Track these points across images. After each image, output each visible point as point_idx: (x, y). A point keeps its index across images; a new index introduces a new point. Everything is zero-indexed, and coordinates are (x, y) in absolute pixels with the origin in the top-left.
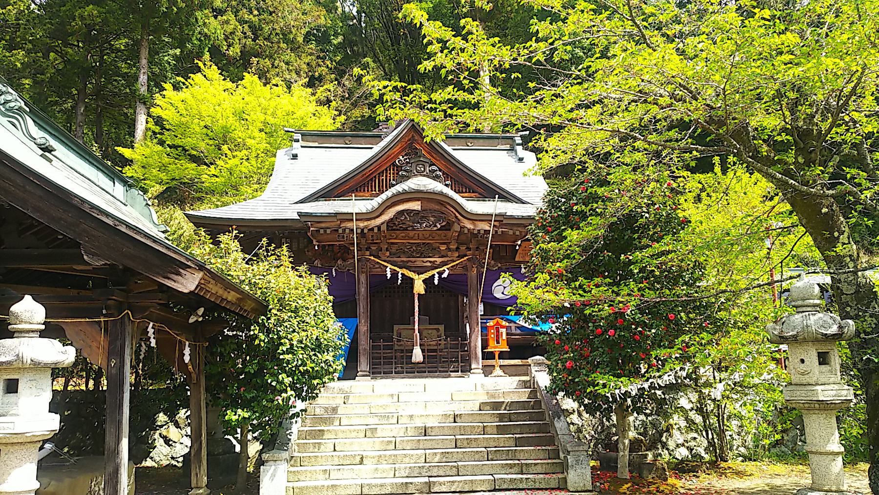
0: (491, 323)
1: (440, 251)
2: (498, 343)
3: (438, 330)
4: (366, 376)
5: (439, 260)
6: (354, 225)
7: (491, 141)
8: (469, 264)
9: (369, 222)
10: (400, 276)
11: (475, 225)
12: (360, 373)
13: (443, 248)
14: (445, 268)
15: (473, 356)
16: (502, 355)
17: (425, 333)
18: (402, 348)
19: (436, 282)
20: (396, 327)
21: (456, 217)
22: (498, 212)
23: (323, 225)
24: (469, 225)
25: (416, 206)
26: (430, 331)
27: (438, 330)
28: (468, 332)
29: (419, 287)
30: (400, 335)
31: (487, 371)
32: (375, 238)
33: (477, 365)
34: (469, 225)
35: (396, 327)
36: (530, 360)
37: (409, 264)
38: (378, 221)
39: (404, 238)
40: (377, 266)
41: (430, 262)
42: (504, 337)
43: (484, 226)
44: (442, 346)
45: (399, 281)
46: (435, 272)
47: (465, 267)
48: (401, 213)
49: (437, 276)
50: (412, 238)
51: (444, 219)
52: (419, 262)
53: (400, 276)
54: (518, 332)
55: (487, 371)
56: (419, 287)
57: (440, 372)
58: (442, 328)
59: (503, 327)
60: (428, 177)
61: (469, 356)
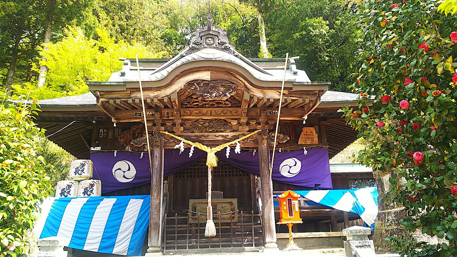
0: (284, 195)
1: (231, 127)
2: (291, 214)
3: (231, 203)
4: (158, 252)
5: (231, 134)
6: (142, 95)
7: (271, 63)
8: (259, 138)
9: (159, 92)
10: (192, 149)
11: (264, 94)
12: (150, 249)
13: (234, 123)
14: (236, 141)
15: (267, 229)
16: (297, 228)
17: (219, 207)
18: (196, 222)
19: (228, 155)
20: (191, 202)
21: (246, 86)
22: (286, 79)
23: (113, 96)
24: (258, 93)
25: (206, 76)
26: (224, 205)
27: (231, 203)
28: (260, 204)
29: (212, 160)
30: (195, 209)
31: (282, 244)
32: (170, 115)
33: (272, 238)
34: (258, 93)
35: (191, 202)
36: (345, 232)
37: (202, 139)
38: (168, 91)
39: (197, 115)
40: (172, 141)
41: (223, 136)
42: (297, 209)
43: (273, 95)
44: (236, 220)
45: (191, 154)
46: (227, 145)
47: (256, 141)
48: (190, 84)
49: (228, 149)
50: (205, 115)
51: (235, 89)
52: (212, 136)
53: (192, 149)
54: (307, 206)
55: (282, 244)
56: (212, 160)
57: (234, 246)
58: (235, 201)
59: (296, 199)
60: (217, 48)
61: (263, 228)
